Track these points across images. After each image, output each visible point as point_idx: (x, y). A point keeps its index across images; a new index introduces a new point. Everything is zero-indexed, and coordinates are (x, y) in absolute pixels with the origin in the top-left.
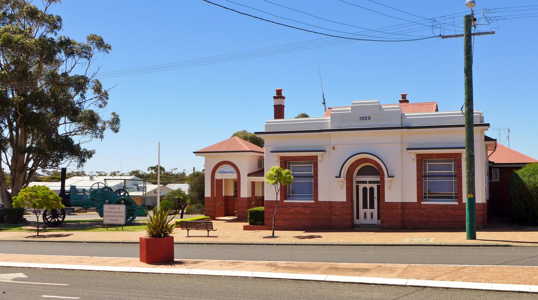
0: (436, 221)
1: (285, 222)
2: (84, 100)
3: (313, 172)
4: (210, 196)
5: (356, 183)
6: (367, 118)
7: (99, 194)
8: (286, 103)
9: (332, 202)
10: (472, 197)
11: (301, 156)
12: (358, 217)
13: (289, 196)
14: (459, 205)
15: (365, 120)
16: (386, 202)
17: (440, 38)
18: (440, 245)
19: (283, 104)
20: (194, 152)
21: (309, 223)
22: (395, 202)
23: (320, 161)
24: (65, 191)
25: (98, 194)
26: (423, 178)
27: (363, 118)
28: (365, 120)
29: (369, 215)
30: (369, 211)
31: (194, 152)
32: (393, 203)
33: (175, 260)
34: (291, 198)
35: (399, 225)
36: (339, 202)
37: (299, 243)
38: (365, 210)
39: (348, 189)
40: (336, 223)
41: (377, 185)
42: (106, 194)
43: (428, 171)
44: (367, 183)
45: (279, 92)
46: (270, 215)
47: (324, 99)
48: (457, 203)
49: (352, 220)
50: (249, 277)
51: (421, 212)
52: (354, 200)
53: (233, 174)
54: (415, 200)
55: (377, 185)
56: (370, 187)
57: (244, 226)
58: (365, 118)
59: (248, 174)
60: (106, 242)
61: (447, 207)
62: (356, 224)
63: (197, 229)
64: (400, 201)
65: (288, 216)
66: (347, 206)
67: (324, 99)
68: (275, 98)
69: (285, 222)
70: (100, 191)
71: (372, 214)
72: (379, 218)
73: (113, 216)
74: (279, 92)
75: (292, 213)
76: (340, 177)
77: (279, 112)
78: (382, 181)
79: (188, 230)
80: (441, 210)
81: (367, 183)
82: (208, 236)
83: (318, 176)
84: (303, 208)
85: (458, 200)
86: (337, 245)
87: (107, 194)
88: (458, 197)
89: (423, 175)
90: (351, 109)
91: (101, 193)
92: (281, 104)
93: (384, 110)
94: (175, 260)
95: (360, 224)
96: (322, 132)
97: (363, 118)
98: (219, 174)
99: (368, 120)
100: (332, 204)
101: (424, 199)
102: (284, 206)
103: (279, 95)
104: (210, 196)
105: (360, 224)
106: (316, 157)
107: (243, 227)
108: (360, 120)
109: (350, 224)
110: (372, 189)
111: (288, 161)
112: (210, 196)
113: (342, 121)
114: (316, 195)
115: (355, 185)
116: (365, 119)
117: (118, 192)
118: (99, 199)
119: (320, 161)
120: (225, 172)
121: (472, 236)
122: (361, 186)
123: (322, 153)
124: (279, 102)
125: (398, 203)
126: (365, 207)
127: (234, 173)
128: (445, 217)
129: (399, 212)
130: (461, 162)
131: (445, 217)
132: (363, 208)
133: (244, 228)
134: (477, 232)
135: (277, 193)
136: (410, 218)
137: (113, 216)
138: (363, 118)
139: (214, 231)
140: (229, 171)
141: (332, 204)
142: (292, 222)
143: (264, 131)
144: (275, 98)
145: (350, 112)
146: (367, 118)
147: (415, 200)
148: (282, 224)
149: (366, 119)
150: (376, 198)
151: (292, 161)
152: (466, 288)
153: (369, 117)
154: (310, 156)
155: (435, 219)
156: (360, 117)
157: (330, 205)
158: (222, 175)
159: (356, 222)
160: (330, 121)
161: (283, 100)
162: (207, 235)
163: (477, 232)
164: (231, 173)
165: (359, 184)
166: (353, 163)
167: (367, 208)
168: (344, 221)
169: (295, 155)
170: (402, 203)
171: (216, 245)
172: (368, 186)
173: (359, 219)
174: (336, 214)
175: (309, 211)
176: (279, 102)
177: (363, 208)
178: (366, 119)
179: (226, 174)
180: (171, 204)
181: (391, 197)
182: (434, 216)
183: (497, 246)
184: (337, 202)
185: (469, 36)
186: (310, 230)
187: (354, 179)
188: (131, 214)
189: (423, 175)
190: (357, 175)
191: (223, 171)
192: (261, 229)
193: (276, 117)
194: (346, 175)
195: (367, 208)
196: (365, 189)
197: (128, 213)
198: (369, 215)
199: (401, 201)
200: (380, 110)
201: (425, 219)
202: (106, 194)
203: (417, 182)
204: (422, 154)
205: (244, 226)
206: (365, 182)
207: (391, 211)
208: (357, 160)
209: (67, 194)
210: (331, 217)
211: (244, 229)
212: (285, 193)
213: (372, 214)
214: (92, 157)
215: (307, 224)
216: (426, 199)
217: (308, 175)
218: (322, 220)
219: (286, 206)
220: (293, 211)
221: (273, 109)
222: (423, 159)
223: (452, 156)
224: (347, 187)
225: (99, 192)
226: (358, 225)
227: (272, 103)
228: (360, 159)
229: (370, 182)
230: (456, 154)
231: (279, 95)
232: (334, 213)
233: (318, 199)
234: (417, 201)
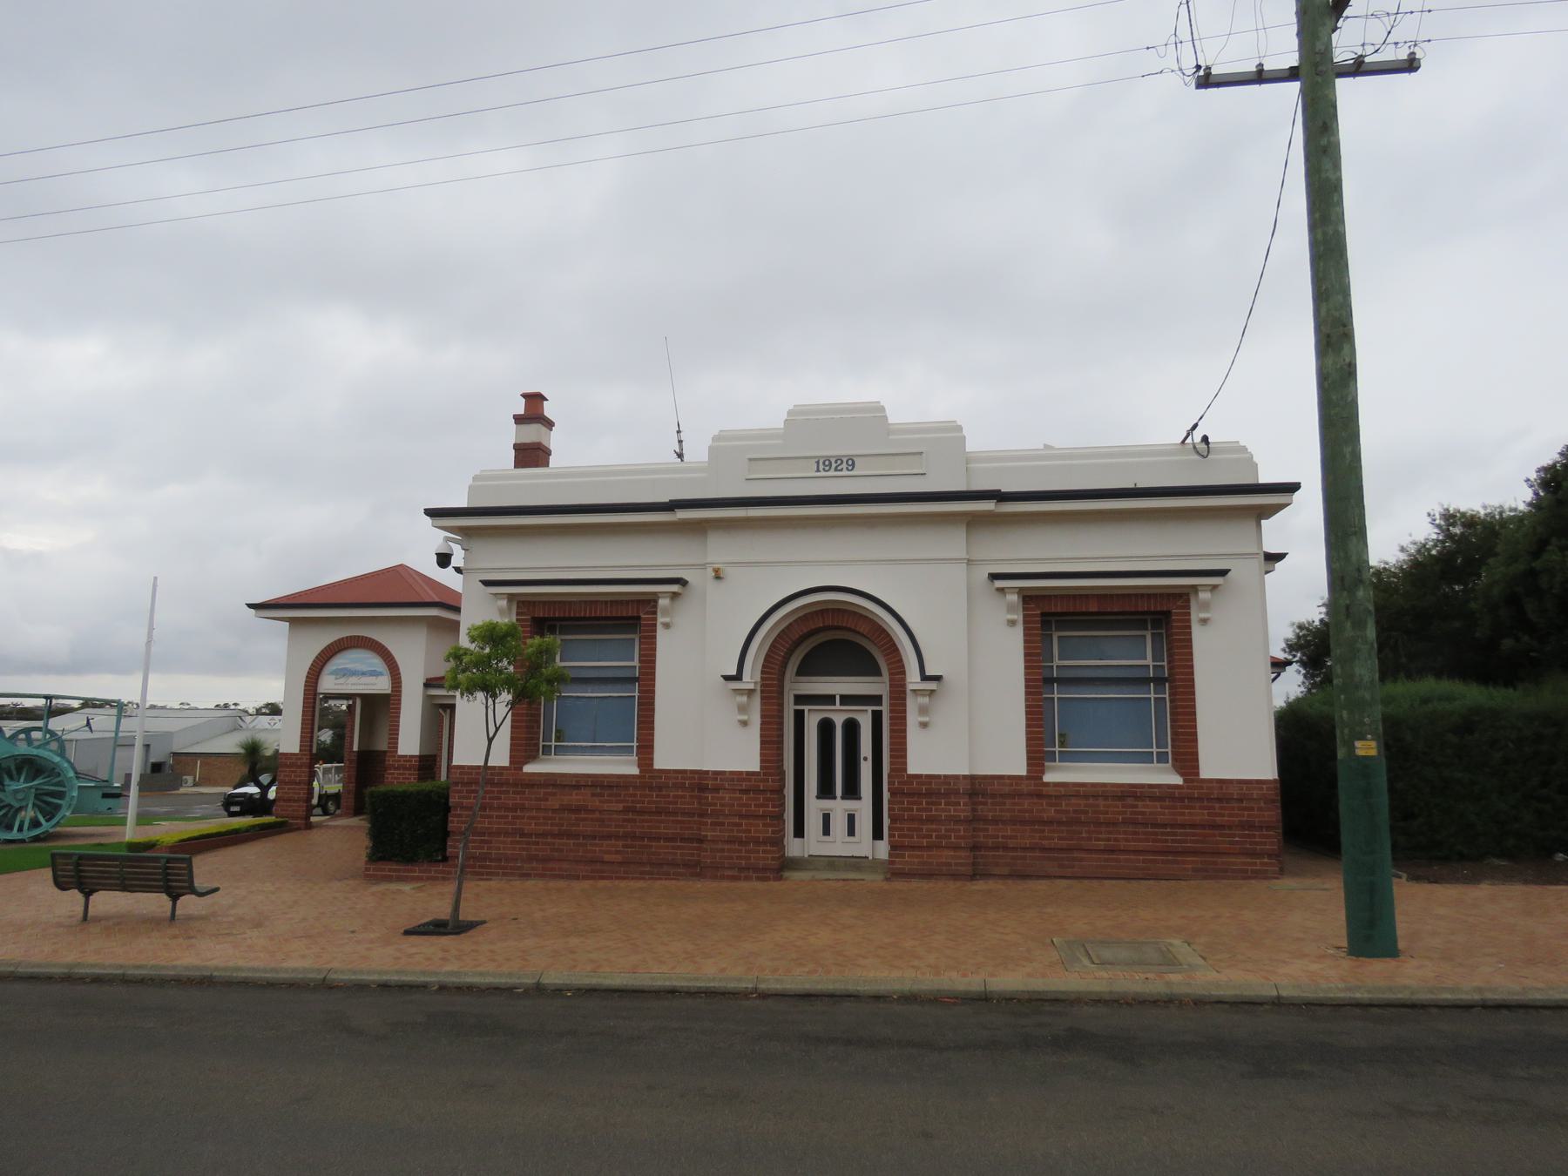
3: (636, 663)
4: (757, 769)
5: (796, 704)
6: (844, 465)
9: (707, 772)
12: (799, 832)
13: (547, 750)
14: (1188, 788)
16: (908, 775)
19: (545, 443)
20: (250, 606)
21: (617, 852)
22: (945, 776)
26: (1166, 675)
27: (827, 464)
29: (839, 825)
30: (839, 807)
31: (250, 606)
32: (938, 777)
35: (961, 864)
38: (827, 804)
39: (769, 723)
40: (718, 854)
41: (873, 711)
43: (1057, 662)
45: (534, 400)
47: (680, 442)
49: (778, 842)
52: (785, 768)
53: (380, 677)
54: (1017, 766)
55: (873, 711)
56: (818, 720)
58: (834, 465)
59: (427, 680)
62: (790, 855)
64: (963, 770)
66: (943, 831)
67: (680, 442)
68: (519, 419)
71: (851, 819)
72: (877, 834)
74: (534, 400)
77: (531, 455)
78: (899, 693)
95: (806, 856)
98: (333, 677)
99: (845, 469)
100: (706, 779)
104: (296, 750)
105: (806, 856)
109: (773, 859)
110: (851, 728)
112: (757, 769)
114: (646, 749)
115: (790, 709)
116: (837, 467)
117: (22, 736)
120: (354, 673)
124: (532, 433)
125: (956, 777)
126: (826, 791)
127: (380, 674)
132: (818, 797)
135: (491, 735)
136: (1003, 837)
138: (827, 463)
139: (201, 895)
140: (365, 668)
144: (519, 419)
146: (844, 465)
147: (1017, 766)
149: (839, 468)
150: (865, 759)
153: (850, 462)
157: (700, 783)
158: (342, 680)
159: (794, 848)
164: (371, 675)
165: (806, 708)
167: (835, 798)
170: (972, 778)
172: (853, 712)
173: (803, 837)
176: (532, 433)
177: (818, 797)
178: (839, 468)
179: (353, 680)
181: (1358, 744)
191: (345, 669)
195: (835, 798)
196: (826, 727)
197: (38, 803)
198: (839, 825)
199: (967, 773)
203: (1027, 700)
206: (828, 699)
210: (699, 829)
212: (532, 739)
213: (851, 819)
216: (1053, 764)
229: (846, 700)
233: (652, 759)
234: (1028, 771)
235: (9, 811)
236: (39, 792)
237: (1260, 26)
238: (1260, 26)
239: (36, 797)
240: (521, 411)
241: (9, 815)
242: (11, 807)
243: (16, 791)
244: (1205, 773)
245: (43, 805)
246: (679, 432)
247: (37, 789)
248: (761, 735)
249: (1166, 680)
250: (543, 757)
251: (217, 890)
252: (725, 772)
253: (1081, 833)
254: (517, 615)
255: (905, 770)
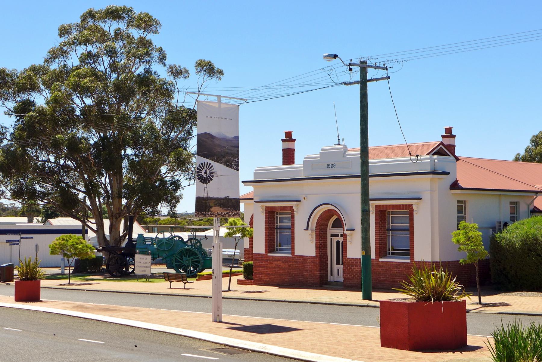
0: (391, 281)
1: (268, 277)
2: (190, 137)
4: (264, 253)
6: (333, 166)
7: (165, 243)
8: (297, 146)
10: (365, 254)
11: (281, 207)
15: (331, 167)
17: (343, 85)
18: (325, 304)
23: (371, 211)
24: (133, 240)
25: (163, 243)
26: (387, 231)
27: (330, 166)
28: (331, 167)
33: (41, 299)
34: (278, 251)
36: (310, 256)
37: (227, 296)
42: (172, 244)
44: (339, 237)
46: (257, 269)
48: (409, 261)
50: (41, 311)
51: (379, 269)
52: (328, 255)
57: (238, 280)
58: (331, 166)
60: (99, 291)
61: (401, 265)
63: (176, 281)
65: (271, 270)
68: (283, 141)
69: (268, 277)
70: (165, 240)
71: (338, 270)
73: (142, 267)
75: (274, 267)
76: (307, 229)
79: (171, 282)
80: (396, 268)
81: (339, 237)
82: (185, 289)
83: (295, 228)
84: (283, 262)
85: (410, 257)
86: (251, 300)
87: (172, 243)
88: (410, 254)
89: (387, 228)
90: (320, 156)
91: (166, 243)
92: (288, 148)
93: (347, 157)
94: (41, 299)
96: (293, 181)
97: (330, 166)
100: (304, 258)
101: (387, 255)
102: (268, 260)
103: (289, 137)
104: (314, 255)
106: (409, 208)
107: (237, 281)
108: (327, 167)
111: (387, 210)
113: (312, 169)
114: (293, 249)
118: (164, 249)
119: (416, 211)
121: (367, 297)
122: (335, 239)
123: (419, 201)
124: (289, 145)
125: (357, 259)
128: (399, 276)
129: (359, 270)
130: (413, 215)
131: (399, 276)
132: (336, 264)
133: (238, 282)
134: (372, 293)
137: (142, 267)
141: (304, 258)
142: (274, 277)
143: (252, 179)
144: (283, 141)
145: (319, 159)
148: (266, 278)
151: (280, 212)
152: (90, 318)
154: (288, 207)
155: (390, 278)
156: (327, 165)
160: (303, 169)
161: (294, 143)
162: (184, 288)
163: (372, 293)
166: (321, 215)
168: (313, 277)
169: (277, 206)
171: (170, 296)
174: (308, 270)
175: (286, 266)
176: (289, 145)
180: (165, 254)
182: (390, 274)
183: (367, 306)
184: (308, 256)
185: (364, 82)
186: (288, 286)
187: (328, 231)
188: (196, 265)
189: (387, 228)
190: (332, 227)
192: (251, 283)
193: (285, 163)
194: (316, 228)
196: (338, 243)
197: (193, 265)
200: (343, 156)
201: (382, 277)
202: (172, 244)
204: (380, 205)
205: (238, 280)
207: (352, 268)
208: (325, 211)
209: (134, 243)
211: (238, 284)
214: (179, 202)
215: (286, 280)
217: (404, 228)
218: (298, 275)
219: (269, 260)
220: (275, 265)
221: (281, 153)
222: (387, 211)
223: (405, 208)
224: (316, 241)
225: (165, 241)
226: (332, 282)
227: (280, 146)
228: (327, 210)
230: (408, 205)
231: (289, 137)
232: (306, 268)
235: (185, 267)
236: (192, 261)
237: (338, 75)
238: (338, 75)
239: (192, 262)
240: (284, 138)
241: (185, 268)
242: (186, 266)
243: (186, 260)
244: (296, 254)
245: (194, 265)
246: (338, 136)
247: (192, 260)
248: (316, 246)
249: (387, 230)
250: (277, 251)
251: (193, 282)
252: (354, 258)
253: (387, 276)
254: (265, 210)
255: (346, 257)
